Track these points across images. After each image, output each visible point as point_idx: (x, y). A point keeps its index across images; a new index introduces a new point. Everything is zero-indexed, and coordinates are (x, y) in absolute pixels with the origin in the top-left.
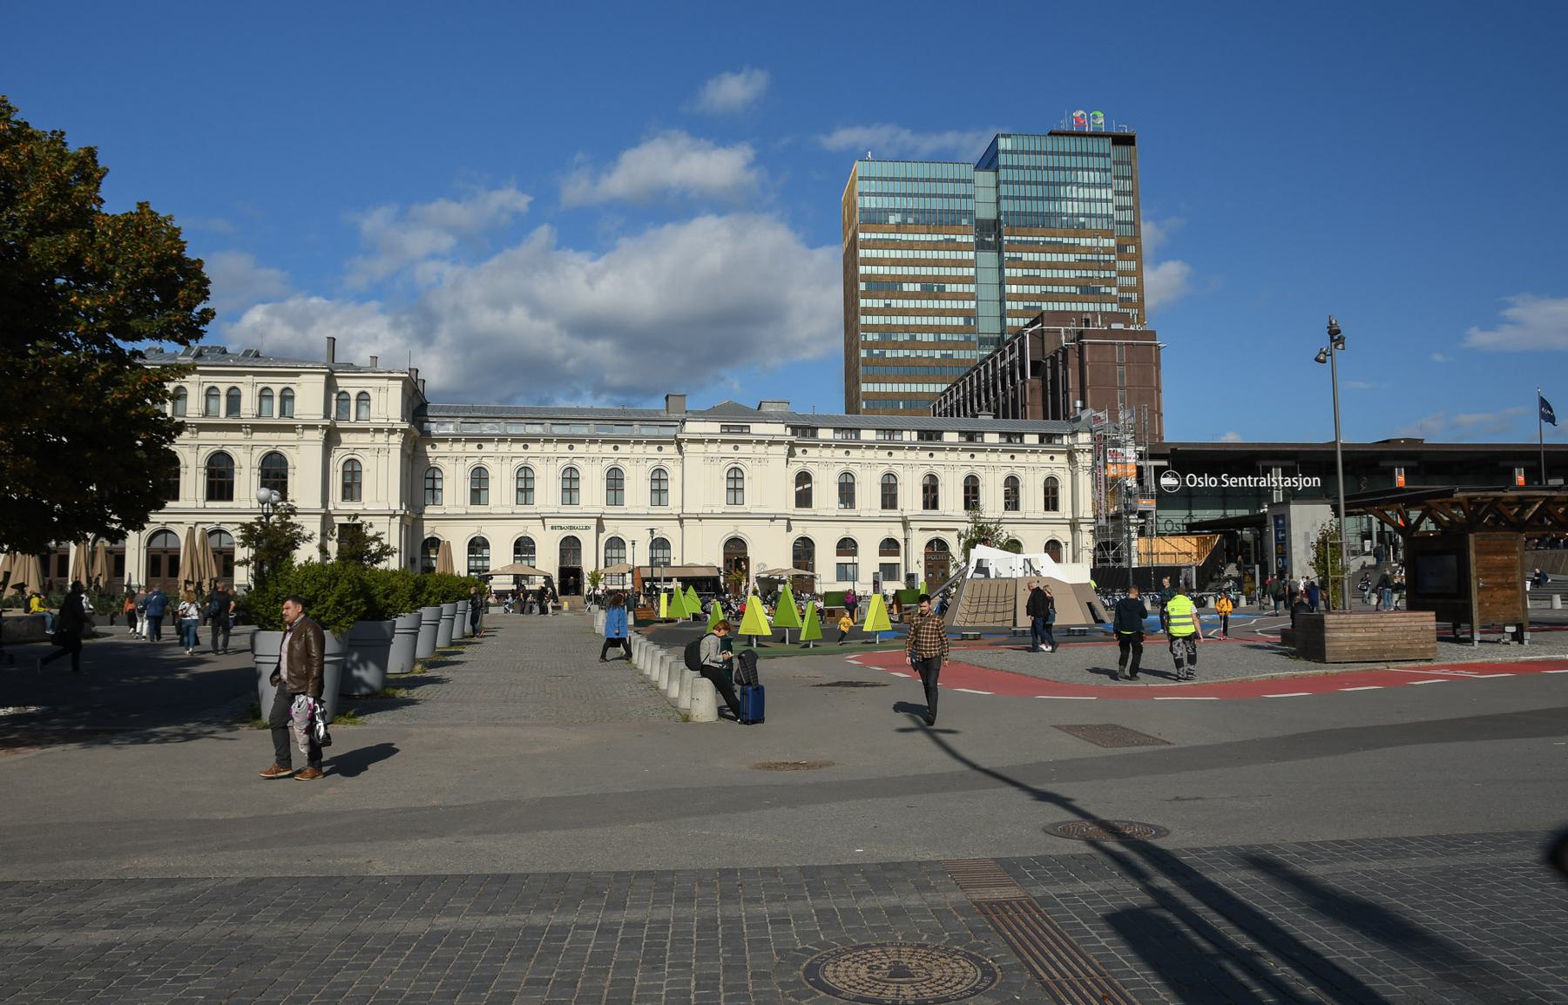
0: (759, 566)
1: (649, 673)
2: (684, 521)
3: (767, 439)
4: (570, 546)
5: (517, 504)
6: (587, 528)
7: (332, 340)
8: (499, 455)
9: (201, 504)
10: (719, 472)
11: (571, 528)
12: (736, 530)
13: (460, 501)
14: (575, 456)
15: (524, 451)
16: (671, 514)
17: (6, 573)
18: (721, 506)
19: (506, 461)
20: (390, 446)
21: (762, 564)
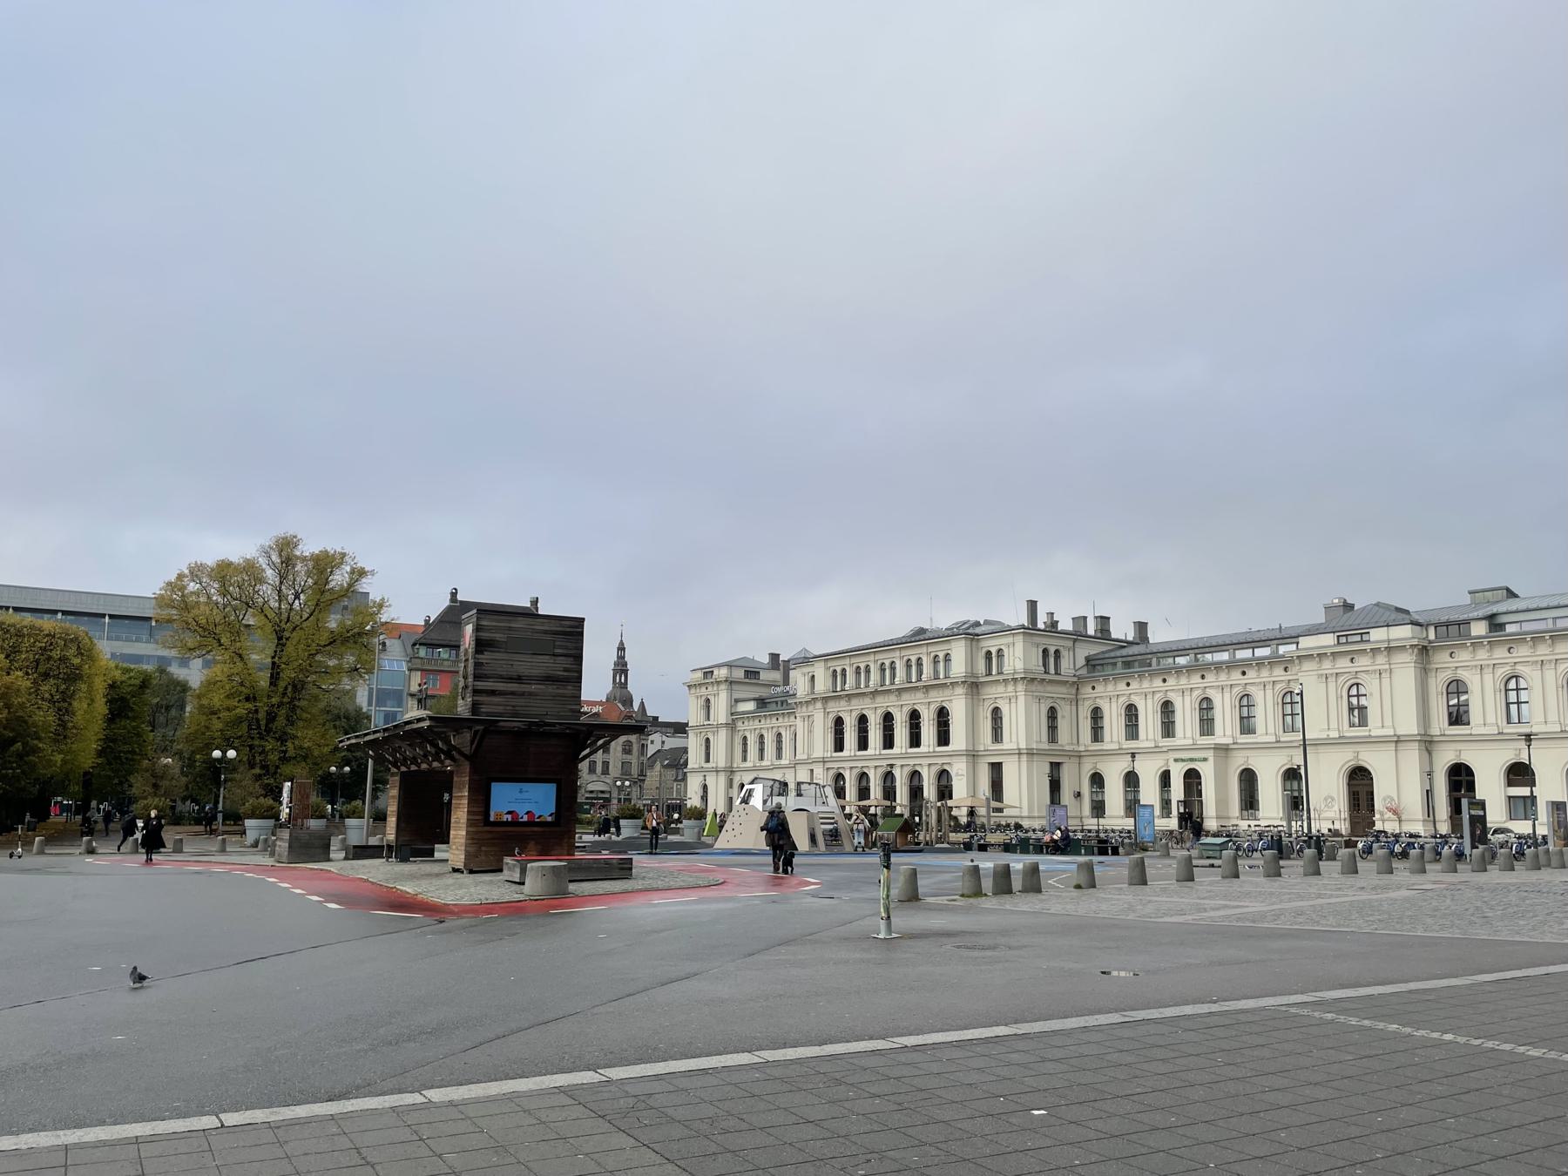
0: (1384, 799)
1: (437, 855)
2: (1137, 755)
3: (1315, 652)
4: (1359, 780)
5: (1284, 732)
6: (1205, 760)
7: (1050, 615)
8: (1180, 687)
9: (904, 751)
10: (1337, 689)
11: (1192, 760)
12: (1095, 767)
13: (1491, 719)
14: (1132, 692)
15: (1242, 677)
16: (1471, 735)
17: (1427, 791)
18: (1045, 746)
19: (1546, 666)
20: (1392, 666)
21: (1389, 797)
